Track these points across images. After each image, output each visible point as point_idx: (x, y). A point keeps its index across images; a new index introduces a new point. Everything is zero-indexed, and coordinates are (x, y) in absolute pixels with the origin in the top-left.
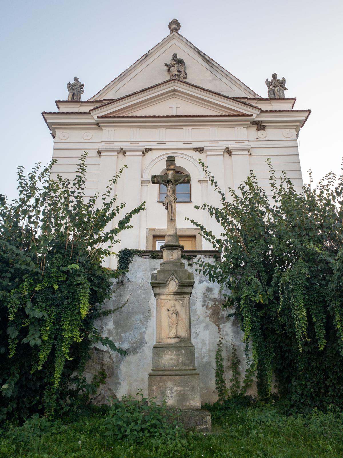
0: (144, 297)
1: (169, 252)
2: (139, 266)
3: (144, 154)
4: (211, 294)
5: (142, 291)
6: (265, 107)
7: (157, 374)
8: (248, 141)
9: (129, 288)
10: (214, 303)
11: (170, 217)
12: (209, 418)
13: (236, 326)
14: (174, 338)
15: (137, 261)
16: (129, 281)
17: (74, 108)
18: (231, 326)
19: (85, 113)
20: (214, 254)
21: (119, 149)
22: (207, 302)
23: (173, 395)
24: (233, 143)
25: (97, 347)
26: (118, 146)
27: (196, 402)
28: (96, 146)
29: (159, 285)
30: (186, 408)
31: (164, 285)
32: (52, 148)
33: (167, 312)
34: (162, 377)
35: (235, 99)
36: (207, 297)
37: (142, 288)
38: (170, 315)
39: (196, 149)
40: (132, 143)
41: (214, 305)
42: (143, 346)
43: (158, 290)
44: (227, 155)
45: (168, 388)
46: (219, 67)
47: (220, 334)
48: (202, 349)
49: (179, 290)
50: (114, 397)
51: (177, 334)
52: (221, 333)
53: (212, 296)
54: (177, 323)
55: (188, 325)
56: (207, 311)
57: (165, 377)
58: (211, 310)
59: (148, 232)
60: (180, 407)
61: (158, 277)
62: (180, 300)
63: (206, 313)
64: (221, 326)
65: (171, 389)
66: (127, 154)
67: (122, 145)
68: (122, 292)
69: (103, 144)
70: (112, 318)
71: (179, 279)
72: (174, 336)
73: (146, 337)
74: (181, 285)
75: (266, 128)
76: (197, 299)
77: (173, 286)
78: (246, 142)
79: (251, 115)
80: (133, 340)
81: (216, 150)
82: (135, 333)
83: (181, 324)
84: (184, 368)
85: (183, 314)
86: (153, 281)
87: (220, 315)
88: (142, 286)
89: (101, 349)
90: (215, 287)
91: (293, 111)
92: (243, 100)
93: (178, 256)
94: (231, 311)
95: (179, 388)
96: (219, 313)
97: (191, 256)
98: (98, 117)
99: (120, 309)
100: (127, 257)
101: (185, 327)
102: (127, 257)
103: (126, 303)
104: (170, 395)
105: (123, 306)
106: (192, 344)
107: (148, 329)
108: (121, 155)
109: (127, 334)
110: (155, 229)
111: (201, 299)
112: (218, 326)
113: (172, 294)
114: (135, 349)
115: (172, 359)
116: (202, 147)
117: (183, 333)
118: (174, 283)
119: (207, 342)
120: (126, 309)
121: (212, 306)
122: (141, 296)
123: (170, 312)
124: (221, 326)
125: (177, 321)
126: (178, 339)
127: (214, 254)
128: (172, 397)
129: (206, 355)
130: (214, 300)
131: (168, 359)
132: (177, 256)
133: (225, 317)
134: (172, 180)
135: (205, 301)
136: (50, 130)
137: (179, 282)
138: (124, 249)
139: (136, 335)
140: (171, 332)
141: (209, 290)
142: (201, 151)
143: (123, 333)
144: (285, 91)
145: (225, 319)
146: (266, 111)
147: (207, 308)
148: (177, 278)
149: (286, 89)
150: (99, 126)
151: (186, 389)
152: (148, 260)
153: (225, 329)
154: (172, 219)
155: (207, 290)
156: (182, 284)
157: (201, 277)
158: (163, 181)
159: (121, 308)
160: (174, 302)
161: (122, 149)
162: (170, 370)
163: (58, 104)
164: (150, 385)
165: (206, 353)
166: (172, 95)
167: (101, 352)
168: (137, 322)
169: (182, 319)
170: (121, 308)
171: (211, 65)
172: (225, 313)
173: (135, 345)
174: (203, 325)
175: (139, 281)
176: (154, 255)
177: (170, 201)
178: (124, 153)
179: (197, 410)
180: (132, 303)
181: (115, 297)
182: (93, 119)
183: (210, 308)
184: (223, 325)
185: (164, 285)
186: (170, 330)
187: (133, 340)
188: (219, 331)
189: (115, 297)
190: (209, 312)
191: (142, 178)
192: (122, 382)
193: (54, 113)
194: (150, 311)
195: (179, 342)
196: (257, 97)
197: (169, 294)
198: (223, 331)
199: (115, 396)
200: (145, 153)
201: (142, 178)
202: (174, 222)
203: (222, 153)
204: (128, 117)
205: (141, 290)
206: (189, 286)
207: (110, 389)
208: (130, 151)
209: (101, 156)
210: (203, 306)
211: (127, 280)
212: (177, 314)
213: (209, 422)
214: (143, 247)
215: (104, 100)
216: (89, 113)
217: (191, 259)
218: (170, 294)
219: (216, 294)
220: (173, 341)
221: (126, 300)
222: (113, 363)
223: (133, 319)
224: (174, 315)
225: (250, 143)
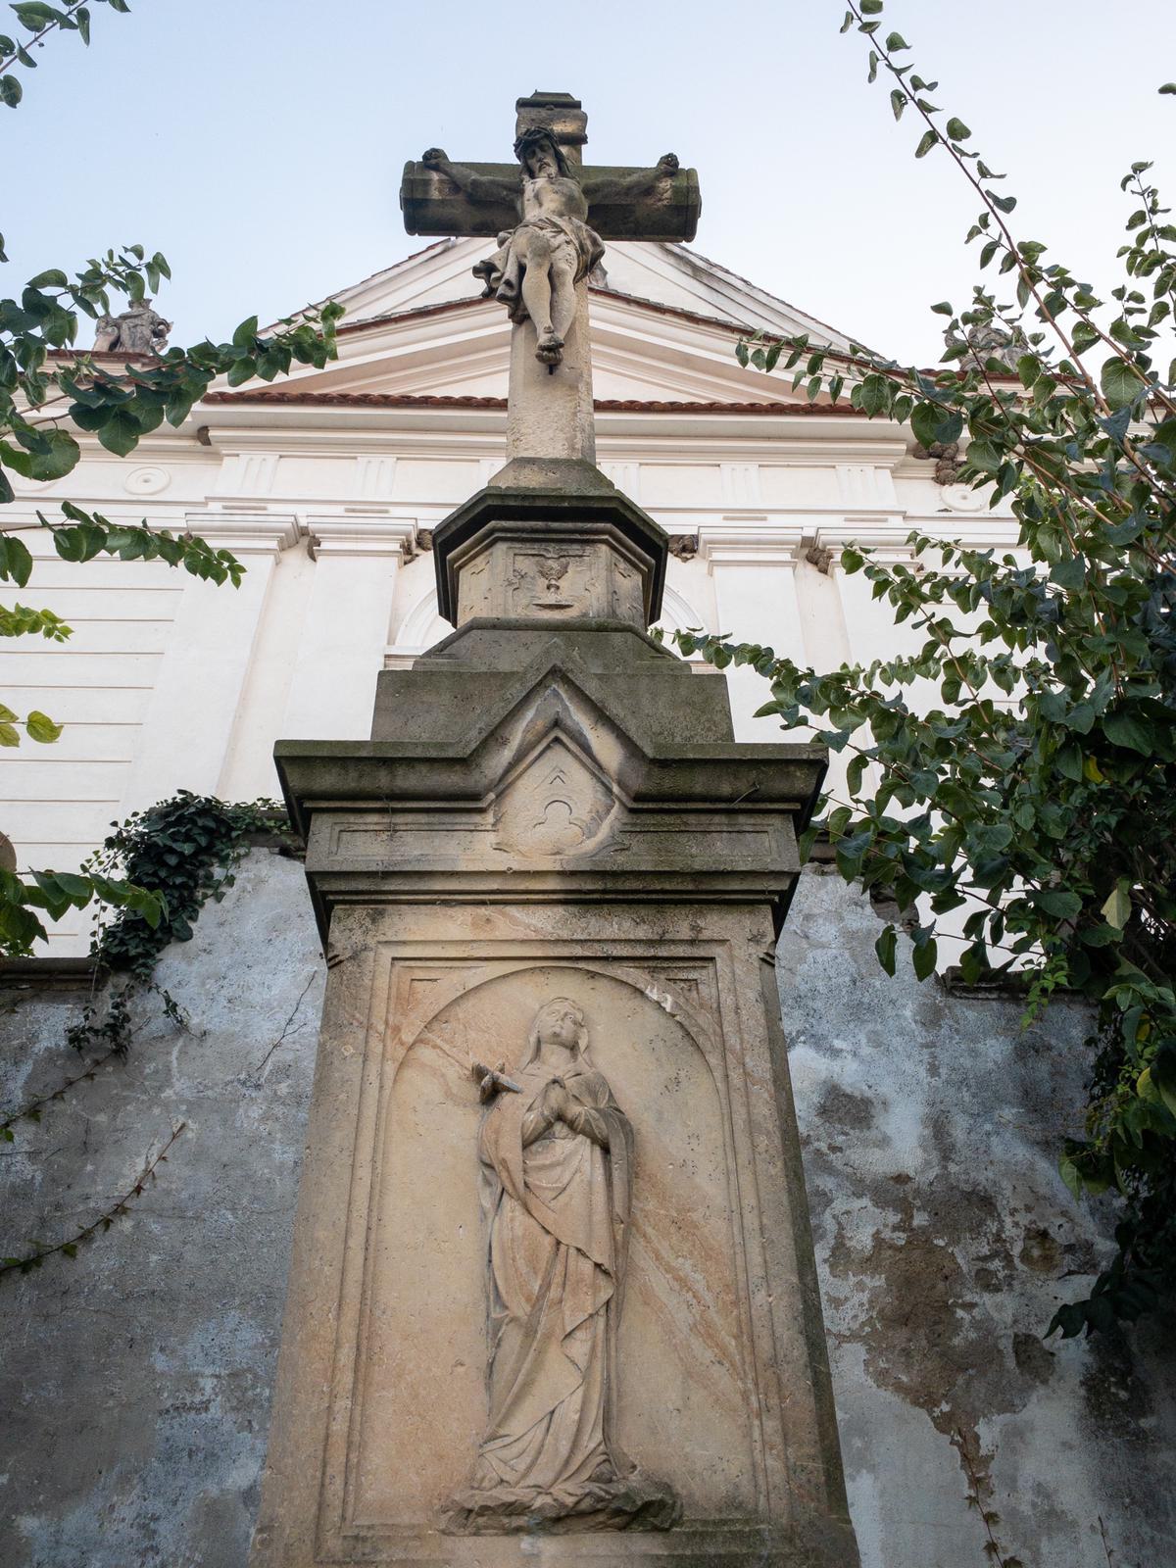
0: (290, 1157)
1: (526, 565)
4: (865, 1143)
5: (279, 1110)
9: (167, 1082)
10: (893, 1218)
13: (1121, 1429)
14: (559, 1521)
16: (181, 1027)
18: (1072, 1435)
22: (839, 1205)
26: (281, 516)
29: (383, 780)
31: (450, 780)
37: (283, 1088)
40: (354, 507)
41: (900, 1238)
46: (746, 289)
47: (990, 1518)
49: (637, 844)
51: (611, 1462)
52: (994, 1504)
53: (877, 1163)
54: (614, 1272)
58: (880, 1281)
62: (654, 964)
64: (981, 1429)
67: (305, 516)
68: (102, 1118)
72: (568, 1492)
82: (156, 1506)
83: (674, 1289)
87: (957, 1326)
90: (887, 1088)
94: (1053, 1287)
96: (949, 1309)
99: (54, 1264)
101: (746, 1332)
102: (187, 849)
103: (121, 1210)
105: (86, 1237)
109: (78, 1518)
112: (957, 1427)
113: (547, 900)
118: (579, 779)
120: (111, 1262)
121: (878, 1241)
122: (267, 1154)
123: (518, 1112)
124: (988, 1433)
130: (893, 1191)
133: (1006, 1345)
138: (170, 794)
140: (522, 1423)
142: (684, 549)
143: (36, 1510)
145: (1011, 1363)
150: (207, 442)
156: (671, 782)
159: (69, 1251)
160: (570, 989)
168: (194, 1388)
169: (683, 1225)
170: (69, 1251)
171: (715, 285)
180: (179, 1212)
181: (33, 1156)
183: (870, 1263)
184: (1000, 1419)
185: (450, 780)
186: (502, 1390)
188: (975, 1482)
191: (391, 641)
198: (1012, 1483)
200: (416, 551)
201: (391, 641)
203: (787, 557)
205: (276, 1098)
206: (757, 804)
208: (341, 534)
211: (160, 1023)
221: (126, 1185)
223: (160, 1363)
224: (574, 1156)
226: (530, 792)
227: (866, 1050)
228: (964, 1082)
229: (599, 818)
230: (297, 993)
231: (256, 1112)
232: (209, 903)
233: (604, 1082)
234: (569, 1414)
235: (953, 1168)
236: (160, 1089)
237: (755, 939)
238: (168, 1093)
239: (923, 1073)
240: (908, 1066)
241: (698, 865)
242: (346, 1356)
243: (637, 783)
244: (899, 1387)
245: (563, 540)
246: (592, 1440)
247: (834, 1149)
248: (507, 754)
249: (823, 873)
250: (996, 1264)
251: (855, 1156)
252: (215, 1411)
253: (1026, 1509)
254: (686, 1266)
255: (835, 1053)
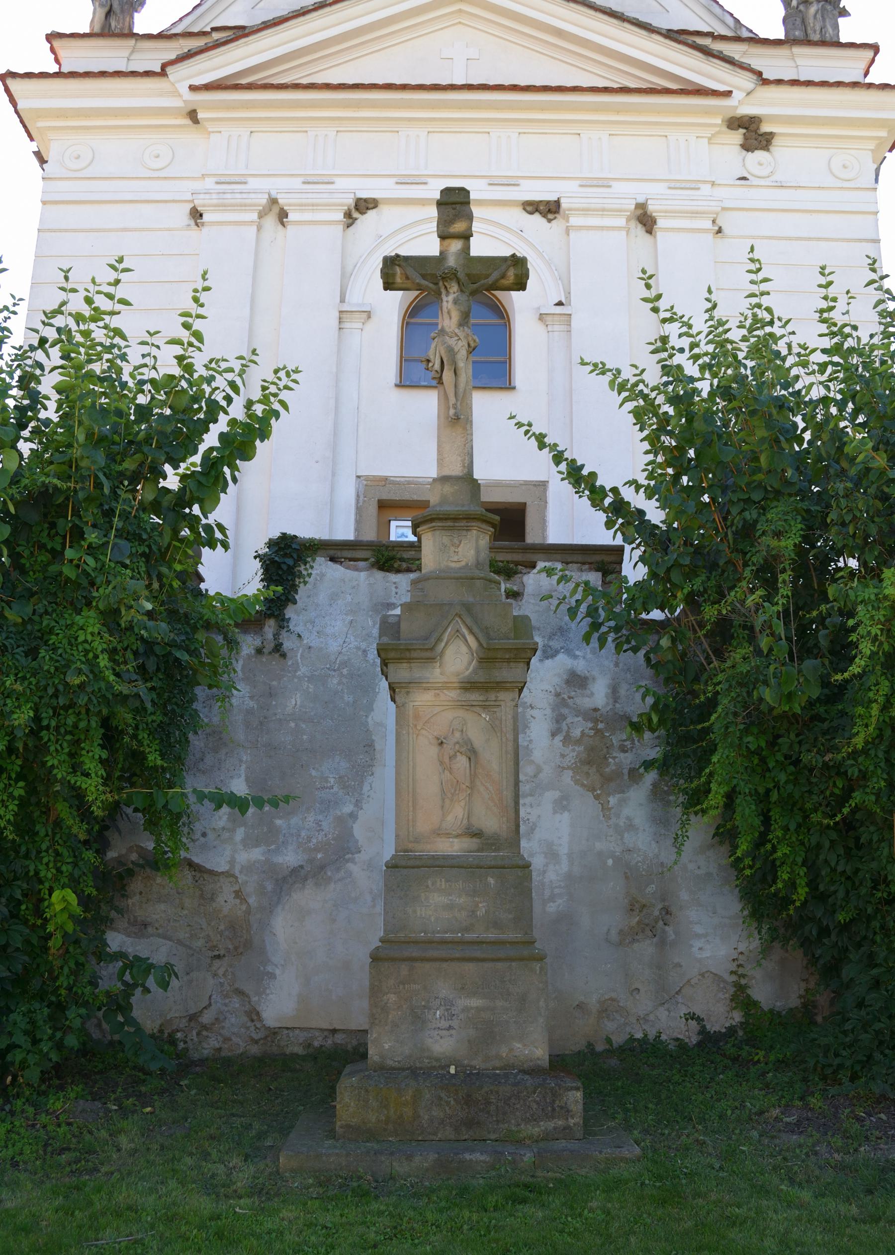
0: (351, 699)
1: (446, 540)
2: (333, 598)
3: (350, 219)
6: (774, 64)
7: (397, 954)
8: (713, 184)
9: (297, 669)
10: (590, 725)
11: (452, 412)
12: (575, 1098)
15: (324, 574)
17: (111, 55)
19: (148, 74)
20: (597, 558)
21: (263, 200)
22: (569, 720)
23: (455, 1023)
24: (659, 189)
25: (196, 860)
27: (536, 1050)
28: (184, 190)
29: (408, 654)
30: (498, 1064)
32: (39, 196)
33: (434, 750)
34: (418, 964)
35: (677, 36)
36: (566, 705)
37: (345, 671)
38: (447, 760)
39: (533, 207)
42: (348, 861)
43: (401, 672)
44: (640, 230)
45: (438, 1002)
48: (545, 872)
50: (254, 1015)
53: (586, 703)
54: (472, 787)
55: (508, 794)
56: (567, 751)
57: (427, 965)
58: (582, 748)
59: (362, 490)
60: (478, 1063)
61: (404, 626)
62: (484, 707)
63: (563, 756)
65: (448, 1004)
66: (292, 217)
68: (275, 683)
69: (209, 183)
70: (244, 766)
71: (480, 636)
73: (358, 831)
74: (489, 657)
75: (775, 141)
76: (534, 712)
77: (457, 658)
78: (706, 189)
79: (728, 94)
80: (314, 841)
81: (603, 210)
82: (320, 817)
84: (491, 935)
85: (493, 756)
86: (385, 640)
87: (608, 765)
88: (344, 664)
89: (208, 866)
90: (595, 673)
91: (870, 86)
92: (700, 41)
93: (478, 552)
95: (475, 1003)
97: (517, 564)
98: (193, 88)
100: (290, 562)
104: (444, 1024)
106: (523, 858)
107: (364, 806)
108: (270, 222)
109: (295, 820)
110: (385, 480)
111: (548, 711)
113: (455, 688)
114: (322, 868)
115: (450, 907)
116: (553, 197)
117: (491, 822)
118: (464, 649)
119: (564, 850)
121: (583, 732)
125: (472, 782)
126: (475, 840)
127: (597, 558)
128: (450, 1028)
129: (557, 891)
130: (593, 715)
131: (439, 907)
132: (472, 552)
133: (626, 771)
134: (461, 275)
135: (559, 719)
136: (32, 139)
137: (480, 645)
139: (324, 824)
141: (577, 681)
142: (550, 211)
143: (280, 818)
144: (841, 20)
145: (626, 777)
146: (779, 82)
147: (567, 740)
148: (476, 629)
149: (844, 13)
151: (499, 1003)
152: (363, 575)
153: (626, 811)
154: (456, 419)
155: (568, 682)
157: (550, 638)
158: (424, 276)
160: (461, 713)
161: (274, 201)
162: (443, 942)
163: (57, 43)
164: (375, 991)
165: (560, 887)
166: (452, 13)
167: (205, 876)
168: (327, 781)
172: (626, 759)
173: (319, 856)
174: (551, 795)
175: (334, 646)
176: (388, 558)
177: (451, 351)
178: (283, 216)
179: (534, 1071)
182: (177, 94)
183: (578, 742)
185: (428, 654)
187: (314, 841)
189: (251, 698)
190: (572, 754)
191: (342, 301)
192: (278, 972)
193: (43, 75)
194: (370, 746)
195: (478, 851)
196: (745, 34)
197: (445, 686)
198: (618, 816)
199: (258, 1014)
201: (342, 301)
202: (465, 429)
204: (296, 86)
207: (240, 992)
209: (203, 224)
210: (553, 735)
212: (472, 754)
213: (573, 1107)
214: (345, 531)
215: (213, 29)
216: (163, 73)
217: (516, 573)
218: (448, 688)
219: (599, 695)
220: (456, 847)
222: (248, 912)
223: (314, 773)
225: (720, 192)
226: (450, 653)
227: (589, 656)
228: (629, 670)
229: (470, 664)
230: (345, 629)
231: (335, 681)
232: (302, 585)
233: (469, 740)
234: (461, 816)
235: (618, 705)
236: (296, 671)
237: (513, 700)
238: (299, 673)
239: (612, 666)
240: (606, 663)
241: (498, 679)
242: (410, 804)
243: (482, 656)
244: (583, 785)
245: (460, 529)
246: (465, 822)
247: (570, 698)
248: (443, 644)
249: (582, 571)
250: (628, 743)
251: (578, 701)
252: (335, 789)
253: (622, 824)
254: (488, 785)
255: (576, 657)
